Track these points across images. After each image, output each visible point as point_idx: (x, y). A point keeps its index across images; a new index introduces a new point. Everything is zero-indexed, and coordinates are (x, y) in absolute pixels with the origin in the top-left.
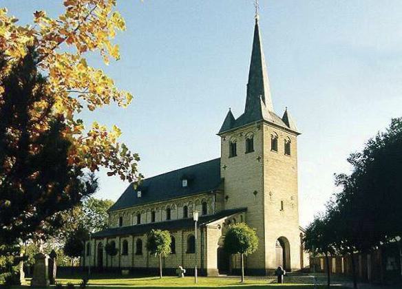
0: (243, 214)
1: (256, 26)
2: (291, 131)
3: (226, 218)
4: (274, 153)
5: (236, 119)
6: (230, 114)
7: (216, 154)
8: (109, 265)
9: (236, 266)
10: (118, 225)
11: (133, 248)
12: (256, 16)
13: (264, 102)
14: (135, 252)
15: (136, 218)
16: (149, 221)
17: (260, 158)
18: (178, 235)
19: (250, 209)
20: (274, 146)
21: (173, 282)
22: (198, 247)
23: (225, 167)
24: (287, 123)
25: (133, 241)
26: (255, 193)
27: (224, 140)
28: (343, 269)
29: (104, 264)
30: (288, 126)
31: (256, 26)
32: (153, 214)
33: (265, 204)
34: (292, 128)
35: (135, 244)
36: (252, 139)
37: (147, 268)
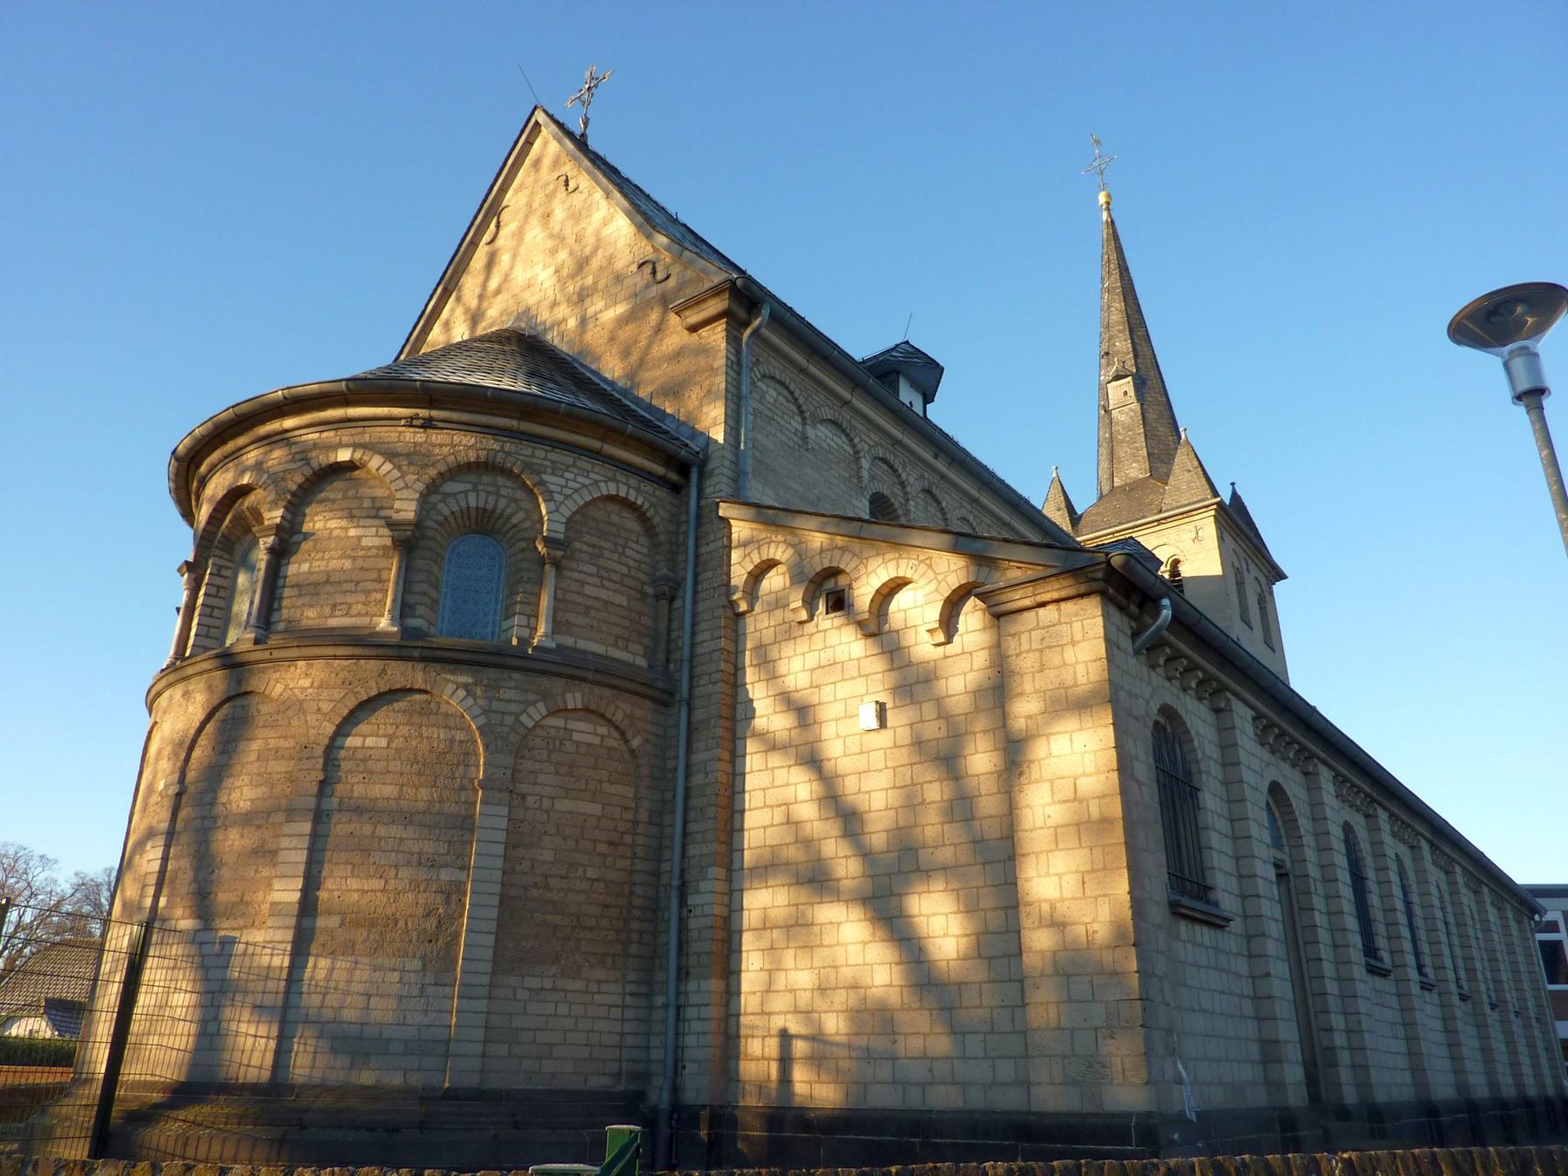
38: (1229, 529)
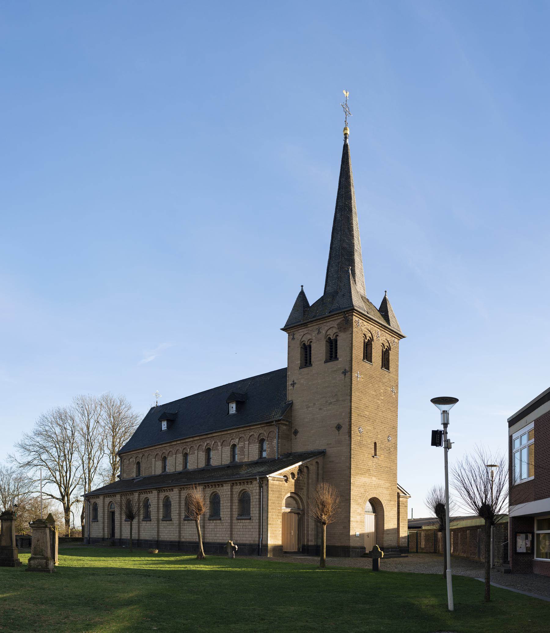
0: (320, 460)
1: (346, 147)
2: (392, 331)
3: (300, 463)
4: (367, 365)
5: (310, 305)
6: (302, 296)
7: (282, 363)
8: (135, 536)
9: (308, 540)
10: (134, 475)
11: (158, 511)
12: (345, 129)
13: (355, 281)
14: (161, 517)
15: (159, 464)
16: (180, 468)
17: (348, 372)
18: (224, 491)
19: (329, 451)
20: (368, 356)
21: (155, 566)
22: (254, 511)
23: (293, 384)
24: (386, 317)
25: (158, 497)
26: (339, 427)
27: (293, 339)
28: (492, 529)
29: (117, 536)
30: (388, 320)
31: (346, 147)
32: (186, 455)
33: (353, 446)
34: (393, 326)
35: (161, 505)
36: (336, 341)
37: (179, 542)
38: (299, 329)
